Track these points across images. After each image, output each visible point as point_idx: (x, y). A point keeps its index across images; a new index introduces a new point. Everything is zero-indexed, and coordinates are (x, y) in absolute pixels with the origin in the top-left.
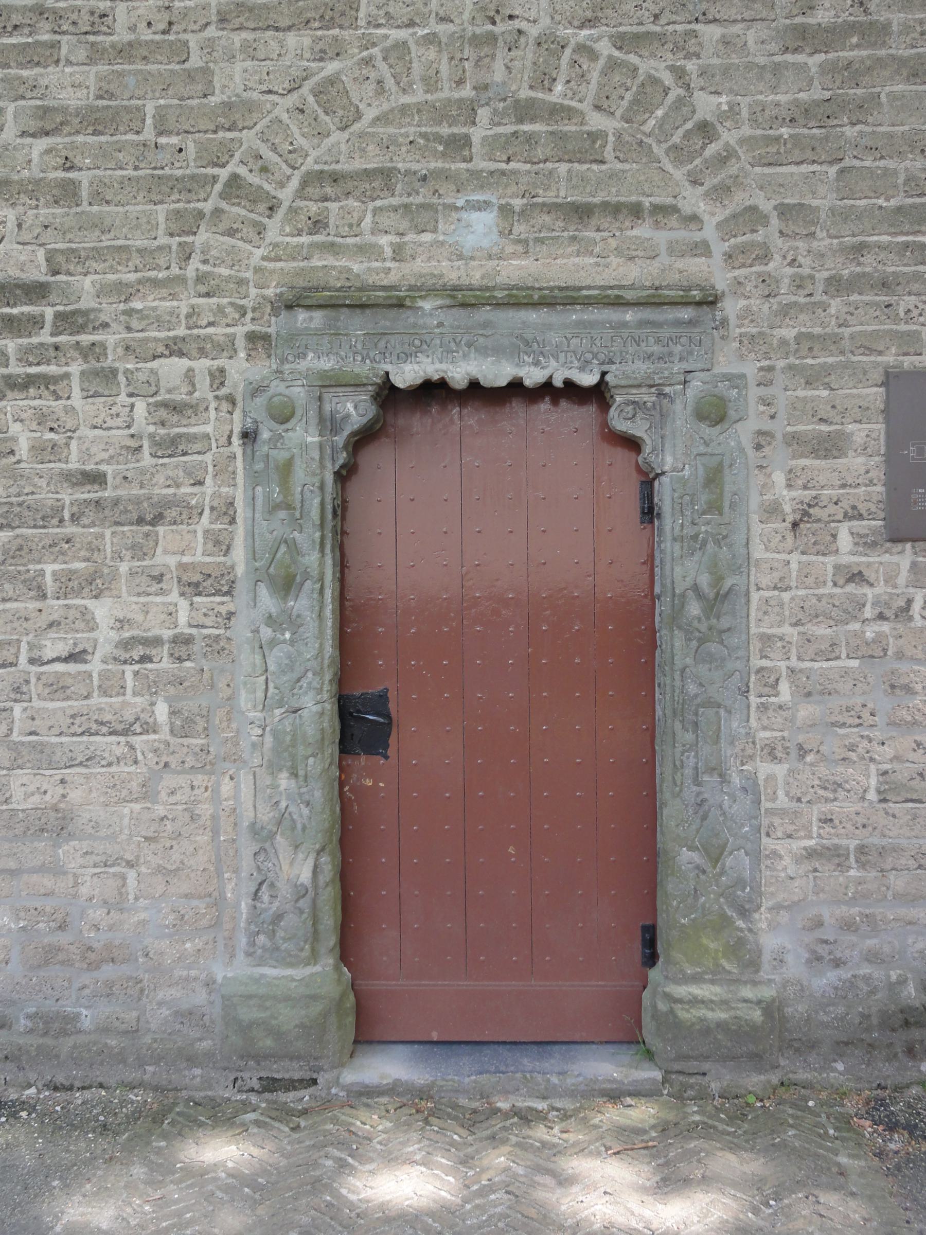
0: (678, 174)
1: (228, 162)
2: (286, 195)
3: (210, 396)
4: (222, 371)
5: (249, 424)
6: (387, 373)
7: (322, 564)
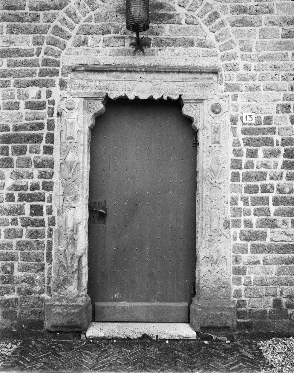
0: (206, 28)
1: (53, 21)
2: (73, 33)
3: (46, 100)
4: (50, 91)
5: (70, 71)
6: (107, 94)
7: (83, 158)
